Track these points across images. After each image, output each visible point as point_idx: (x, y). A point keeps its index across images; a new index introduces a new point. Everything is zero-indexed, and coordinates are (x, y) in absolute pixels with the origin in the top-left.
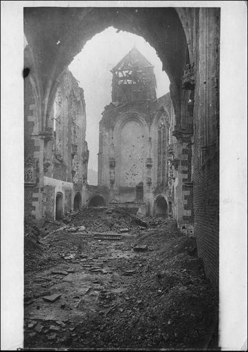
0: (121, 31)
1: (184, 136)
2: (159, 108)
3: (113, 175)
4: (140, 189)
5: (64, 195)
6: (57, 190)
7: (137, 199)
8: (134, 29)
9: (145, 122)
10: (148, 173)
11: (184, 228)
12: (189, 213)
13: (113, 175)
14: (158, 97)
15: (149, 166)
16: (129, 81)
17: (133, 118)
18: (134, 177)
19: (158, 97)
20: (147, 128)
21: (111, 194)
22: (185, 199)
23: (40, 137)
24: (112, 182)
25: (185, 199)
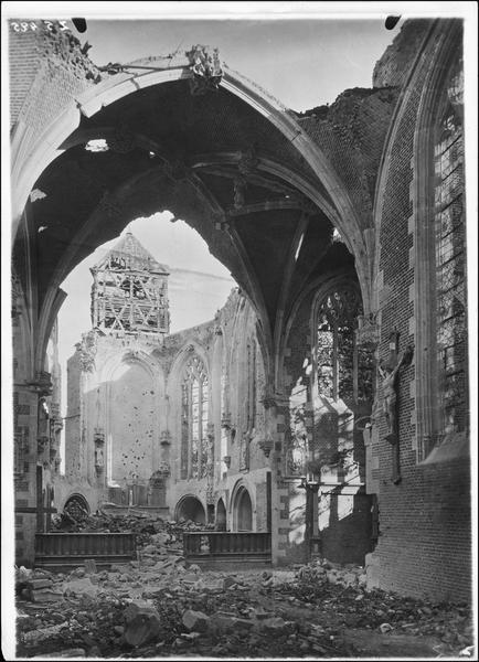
10: (165, 455)
15: (165, 444)
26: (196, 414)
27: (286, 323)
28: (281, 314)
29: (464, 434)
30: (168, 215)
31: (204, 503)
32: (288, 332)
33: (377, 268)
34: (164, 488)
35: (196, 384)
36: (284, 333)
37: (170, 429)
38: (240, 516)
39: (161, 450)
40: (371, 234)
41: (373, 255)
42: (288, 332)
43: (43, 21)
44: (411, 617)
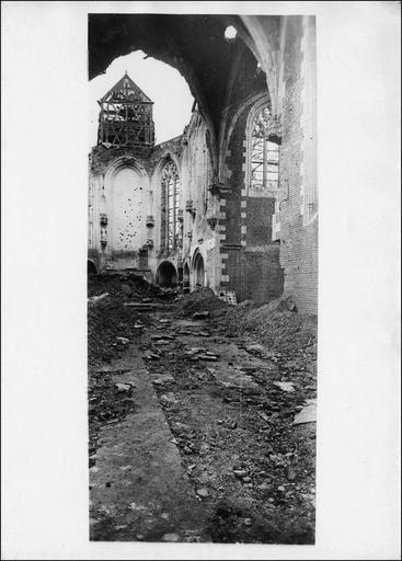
0: (151, 59)
1: (222, 191)
2: (164, 155)
3: (104, 234)
4: (143, 253)
7: (141, 265)
8: (175, 60)
9: (144, 171)
10: (149, 234)
11: (222, 295)
12: (226, 278)
13: (104, 234)
14: (156, 144)
15: (150, 226)
16: (118, 118)
17: (128, 164)
18: (130, 238)
19: (156, 144)
20: (147, 178)
21: (102, 260)
24: (104, 244)
26: (171, 193)
27: (226, 131)
28: (224, 125)
29: (290, 539)
30: (138, 55)
31: (176, 265)
32: (229, 138)
33: (281, 79)
34: (147, 256)
35: (172, 182)
36: (226, 138)
37: (154, 215)
38: (198, 276)
39: (146, 230)
40: (276, 55)
41: (278, 72)
42: (229, 138)
43: (315, 437)
44: (267, 530)
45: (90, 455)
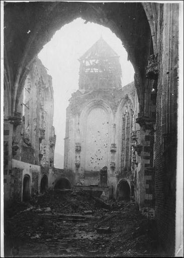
3: (78, 159)
5: (31, 177)
6: (24, 173)
10: (113, 158)
15: (113, 151)
18: (98, 162)
22: (147, 183)
23: (10, 121)
25: (147, 183)
39: (110, 154)
45: (19, 160)
